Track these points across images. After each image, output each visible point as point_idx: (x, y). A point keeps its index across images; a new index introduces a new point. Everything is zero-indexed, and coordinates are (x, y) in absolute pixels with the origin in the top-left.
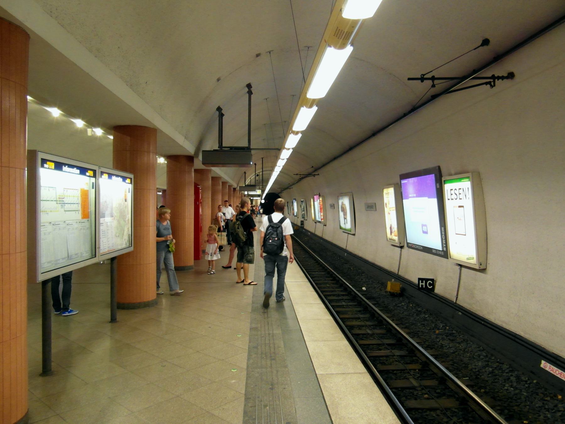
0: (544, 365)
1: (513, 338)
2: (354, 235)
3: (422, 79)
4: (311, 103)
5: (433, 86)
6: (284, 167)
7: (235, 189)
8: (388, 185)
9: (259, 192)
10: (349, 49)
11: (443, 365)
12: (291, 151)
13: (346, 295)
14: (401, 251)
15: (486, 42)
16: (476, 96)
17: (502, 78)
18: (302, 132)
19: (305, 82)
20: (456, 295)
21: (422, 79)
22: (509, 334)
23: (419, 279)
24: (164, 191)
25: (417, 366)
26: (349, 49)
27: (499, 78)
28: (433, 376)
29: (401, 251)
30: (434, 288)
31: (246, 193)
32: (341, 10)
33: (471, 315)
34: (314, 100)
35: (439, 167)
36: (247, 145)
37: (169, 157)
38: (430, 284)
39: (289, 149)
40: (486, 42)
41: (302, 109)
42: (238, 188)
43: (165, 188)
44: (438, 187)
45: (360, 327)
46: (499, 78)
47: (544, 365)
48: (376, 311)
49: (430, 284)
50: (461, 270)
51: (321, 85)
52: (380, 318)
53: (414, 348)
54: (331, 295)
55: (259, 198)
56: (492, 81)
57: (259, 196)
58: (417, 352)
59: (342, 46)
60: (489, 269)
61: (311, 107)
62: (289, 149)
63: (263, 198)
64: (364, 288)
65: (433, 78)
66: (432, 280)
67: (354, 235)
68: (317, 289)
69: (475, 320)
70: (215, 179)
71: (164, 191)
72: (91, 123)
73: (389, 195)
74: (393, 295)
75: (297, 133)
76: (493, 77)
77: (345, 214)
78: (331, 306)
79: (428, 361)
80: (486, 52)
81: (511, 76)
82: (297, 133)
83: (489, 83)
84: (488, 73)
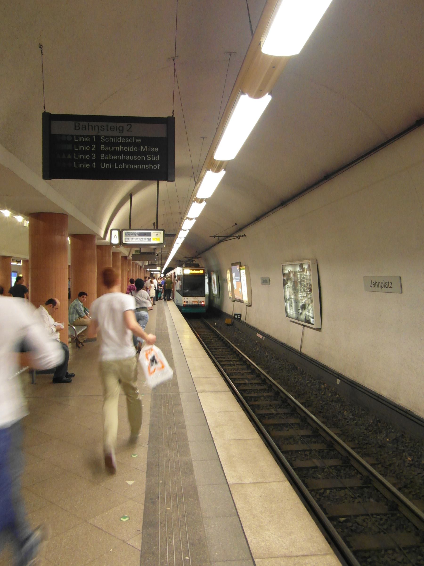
0: (258, 335)
1: (323, 368)
3: (215, 237)
4: (217, 166)
5: (218, 239)
6: (186, 238)
7: (141, 267)
9: (159, 268)
10: (267, 99)
11: (308, 410)
12: (194, 221)
13: (241, 364)
15: (236, 224)
16: (233, 242)
17: (242, 236)
18: (207, 200)
19: (253, 34)
20: (300, 346)
21: (215, 237)
22: (399, 409)
23: (235, 314)
24: (26, 261)
25: (356, 482)
26: (267, 99)
27: (241, 236)
28: (229, 347)
30: (241, 318)
31: (148, 269)
32: (260, 44)
33: (369, 392)
34: (222, 162)
37: (73, 236)
38: (239, 316)
39: (191, 219)
40: (236, 224)
41: (193, 203)
42: (143, 266)
43: (27, 257)
45: (237, 374)
46: (241, 236)
47: (258, 335)
48: (267, 378)
49: (239, 316)
50: (304, 328)
51: (231, 144)
52: (226, 342)
53: (396, 501)
54: (221, 357)
55: (159, 273)
57: (158, 271)
58: (402, 509)
59: (259, 95)
61: (218, 171)
62: (191, 219)
63: (163, 272)
64: (215, 324)
65: (218, 237)
66: (240, 314)
68: (198, 335)
69: (318, 367)
70: (136, 264)
71: (26, 261)
72: (16, 210)
74: (228, 325)
75: (201, 201)
76: (239, 236)
77: (215, 287)
78: (231, 379)
79: (396, 501)
81: (245, 235)
82: (201, 201)
83: (238, 238)
84: (237, 235)
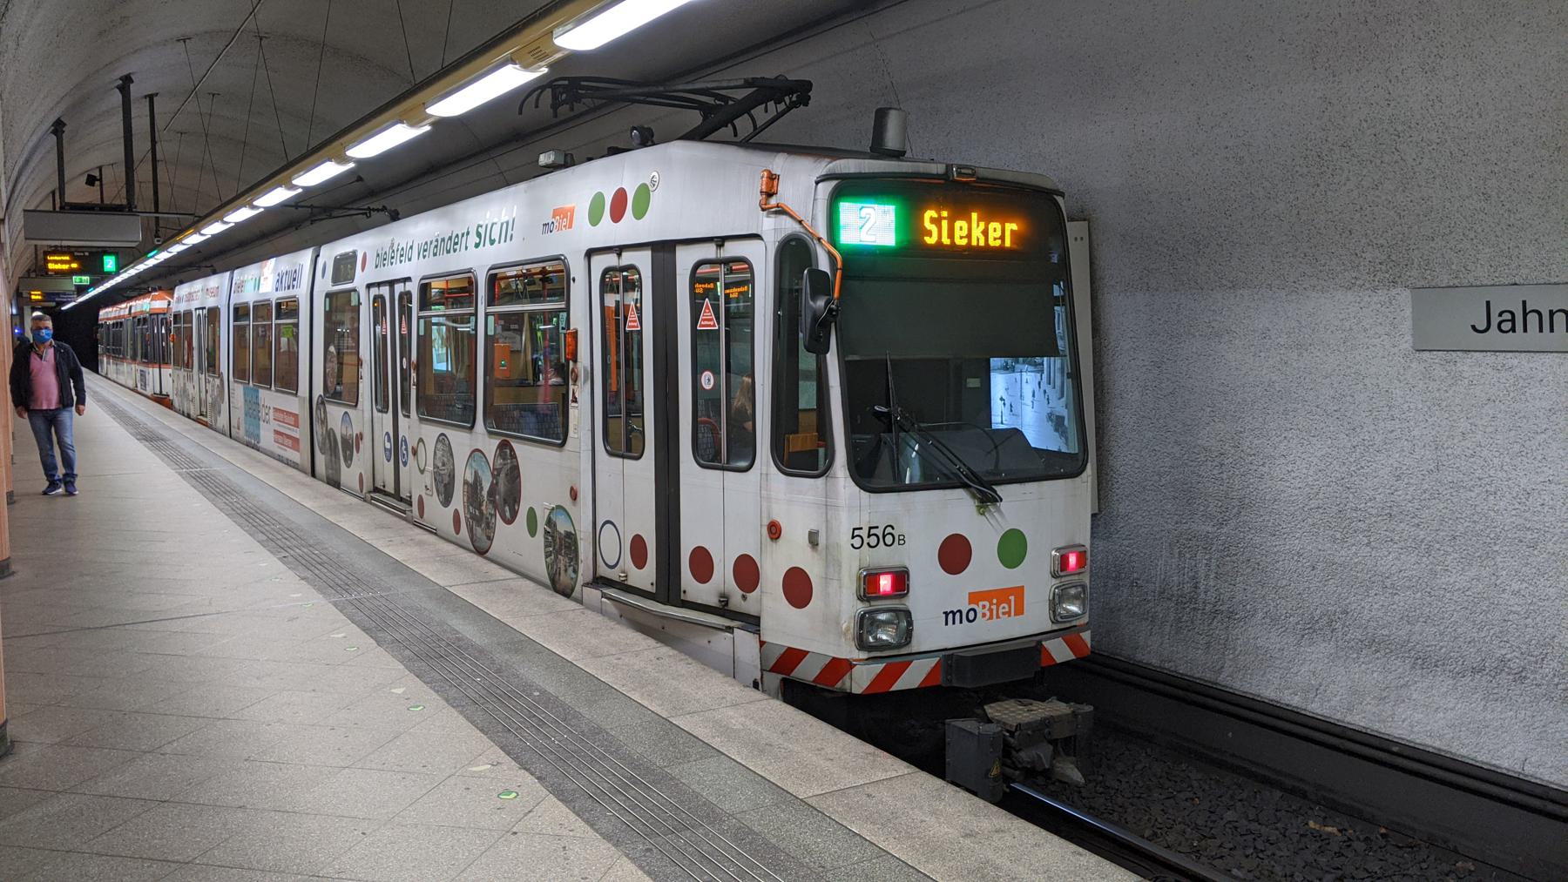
84: (364, 204)
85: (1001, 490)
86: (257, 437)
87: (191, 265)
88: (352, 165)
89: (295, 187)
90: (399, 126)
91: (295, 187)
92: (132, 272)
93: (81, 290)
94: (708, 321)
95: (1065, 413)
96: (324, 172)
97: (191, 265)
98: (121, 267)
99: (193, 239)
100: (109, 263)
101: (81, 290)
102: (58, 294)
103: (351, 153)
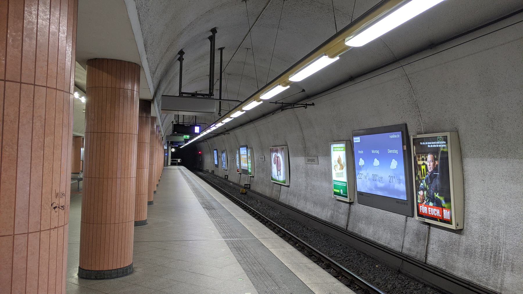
2: (288, 186)
8: (338, 141)
14: (350, 206)
17: (310, 105)
21: (276, 103)
27: (308, 105)
29: (350, 206)
35: (406, 124)
36: (408, 218)
40: (304, 90)
44: (405, 148)
46: (308, 105)
56: (306, 106)
60: (466, 232)
67: (288, 186)
69: (464, 287)
73: (338, 153)
76: (306, 104)
80: (302, 95)
81: (313, 104)
84: (304, 102)
85: (224, 177)
86: (47, 18)
87: (222, 133)
88: (244, 112)
89: (243, 111)
90: (279, 86)
91: (243, 111)
92: (205, 133)
93: (186, 141)
94: (417, 178)
95: (83, 135)
96: (252, 105)
97: (222, 133)
98: (201, 131)
99: (213, 128)
100: (197, 129)
101: (186, 141)
102: (179, 142)
103: (244, 109)
